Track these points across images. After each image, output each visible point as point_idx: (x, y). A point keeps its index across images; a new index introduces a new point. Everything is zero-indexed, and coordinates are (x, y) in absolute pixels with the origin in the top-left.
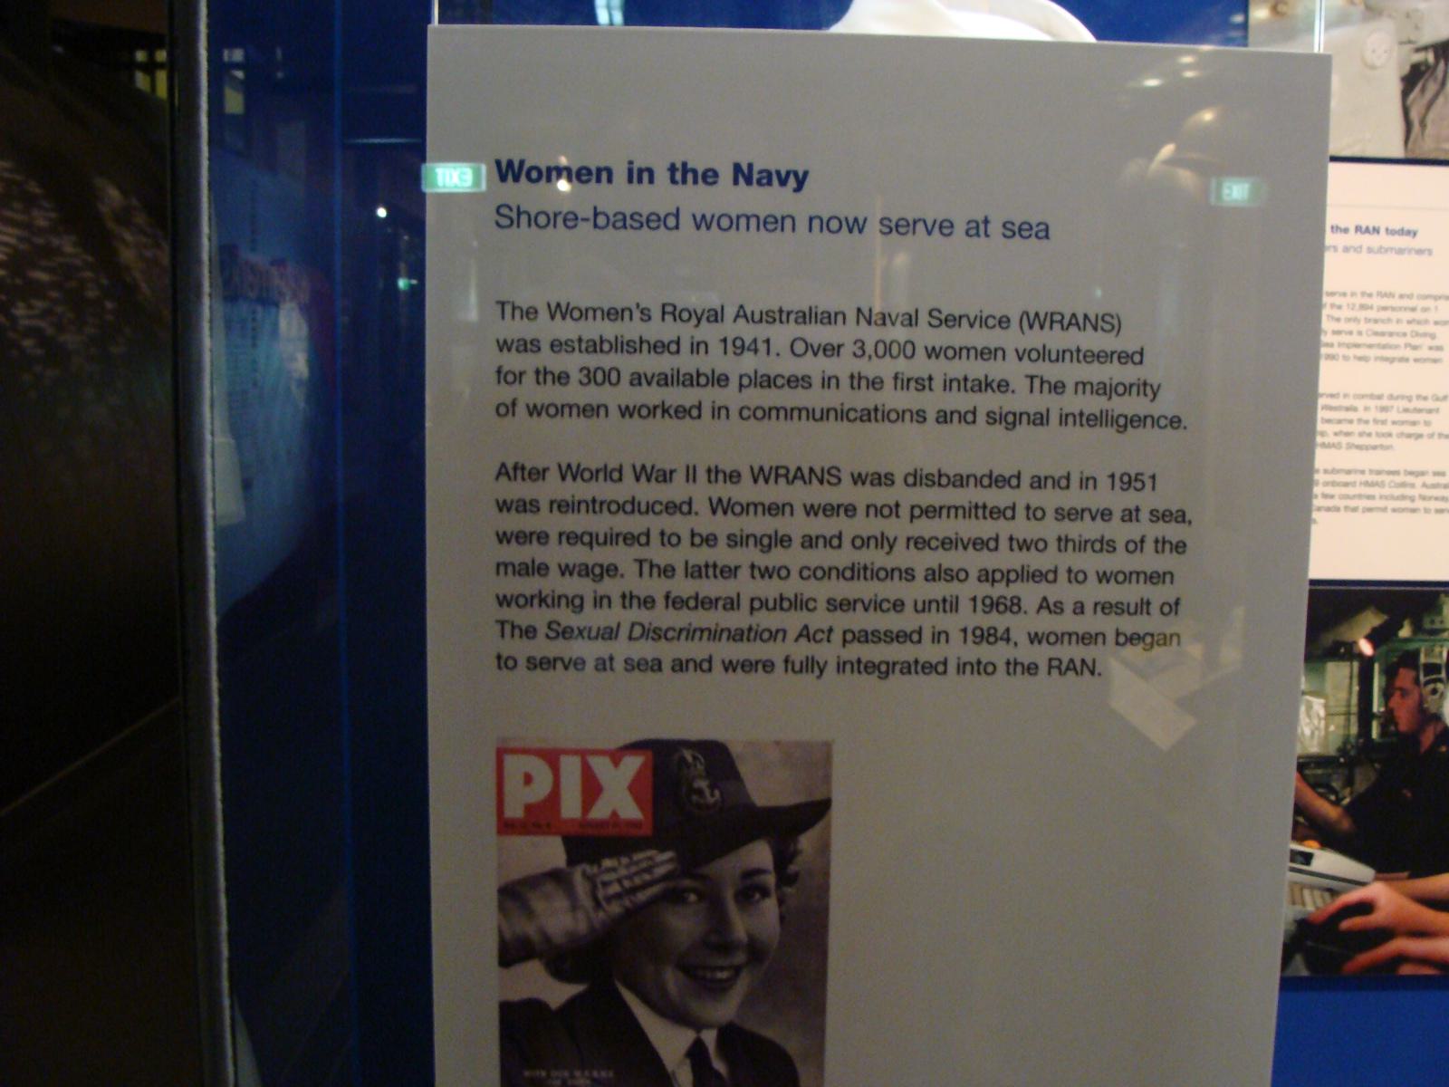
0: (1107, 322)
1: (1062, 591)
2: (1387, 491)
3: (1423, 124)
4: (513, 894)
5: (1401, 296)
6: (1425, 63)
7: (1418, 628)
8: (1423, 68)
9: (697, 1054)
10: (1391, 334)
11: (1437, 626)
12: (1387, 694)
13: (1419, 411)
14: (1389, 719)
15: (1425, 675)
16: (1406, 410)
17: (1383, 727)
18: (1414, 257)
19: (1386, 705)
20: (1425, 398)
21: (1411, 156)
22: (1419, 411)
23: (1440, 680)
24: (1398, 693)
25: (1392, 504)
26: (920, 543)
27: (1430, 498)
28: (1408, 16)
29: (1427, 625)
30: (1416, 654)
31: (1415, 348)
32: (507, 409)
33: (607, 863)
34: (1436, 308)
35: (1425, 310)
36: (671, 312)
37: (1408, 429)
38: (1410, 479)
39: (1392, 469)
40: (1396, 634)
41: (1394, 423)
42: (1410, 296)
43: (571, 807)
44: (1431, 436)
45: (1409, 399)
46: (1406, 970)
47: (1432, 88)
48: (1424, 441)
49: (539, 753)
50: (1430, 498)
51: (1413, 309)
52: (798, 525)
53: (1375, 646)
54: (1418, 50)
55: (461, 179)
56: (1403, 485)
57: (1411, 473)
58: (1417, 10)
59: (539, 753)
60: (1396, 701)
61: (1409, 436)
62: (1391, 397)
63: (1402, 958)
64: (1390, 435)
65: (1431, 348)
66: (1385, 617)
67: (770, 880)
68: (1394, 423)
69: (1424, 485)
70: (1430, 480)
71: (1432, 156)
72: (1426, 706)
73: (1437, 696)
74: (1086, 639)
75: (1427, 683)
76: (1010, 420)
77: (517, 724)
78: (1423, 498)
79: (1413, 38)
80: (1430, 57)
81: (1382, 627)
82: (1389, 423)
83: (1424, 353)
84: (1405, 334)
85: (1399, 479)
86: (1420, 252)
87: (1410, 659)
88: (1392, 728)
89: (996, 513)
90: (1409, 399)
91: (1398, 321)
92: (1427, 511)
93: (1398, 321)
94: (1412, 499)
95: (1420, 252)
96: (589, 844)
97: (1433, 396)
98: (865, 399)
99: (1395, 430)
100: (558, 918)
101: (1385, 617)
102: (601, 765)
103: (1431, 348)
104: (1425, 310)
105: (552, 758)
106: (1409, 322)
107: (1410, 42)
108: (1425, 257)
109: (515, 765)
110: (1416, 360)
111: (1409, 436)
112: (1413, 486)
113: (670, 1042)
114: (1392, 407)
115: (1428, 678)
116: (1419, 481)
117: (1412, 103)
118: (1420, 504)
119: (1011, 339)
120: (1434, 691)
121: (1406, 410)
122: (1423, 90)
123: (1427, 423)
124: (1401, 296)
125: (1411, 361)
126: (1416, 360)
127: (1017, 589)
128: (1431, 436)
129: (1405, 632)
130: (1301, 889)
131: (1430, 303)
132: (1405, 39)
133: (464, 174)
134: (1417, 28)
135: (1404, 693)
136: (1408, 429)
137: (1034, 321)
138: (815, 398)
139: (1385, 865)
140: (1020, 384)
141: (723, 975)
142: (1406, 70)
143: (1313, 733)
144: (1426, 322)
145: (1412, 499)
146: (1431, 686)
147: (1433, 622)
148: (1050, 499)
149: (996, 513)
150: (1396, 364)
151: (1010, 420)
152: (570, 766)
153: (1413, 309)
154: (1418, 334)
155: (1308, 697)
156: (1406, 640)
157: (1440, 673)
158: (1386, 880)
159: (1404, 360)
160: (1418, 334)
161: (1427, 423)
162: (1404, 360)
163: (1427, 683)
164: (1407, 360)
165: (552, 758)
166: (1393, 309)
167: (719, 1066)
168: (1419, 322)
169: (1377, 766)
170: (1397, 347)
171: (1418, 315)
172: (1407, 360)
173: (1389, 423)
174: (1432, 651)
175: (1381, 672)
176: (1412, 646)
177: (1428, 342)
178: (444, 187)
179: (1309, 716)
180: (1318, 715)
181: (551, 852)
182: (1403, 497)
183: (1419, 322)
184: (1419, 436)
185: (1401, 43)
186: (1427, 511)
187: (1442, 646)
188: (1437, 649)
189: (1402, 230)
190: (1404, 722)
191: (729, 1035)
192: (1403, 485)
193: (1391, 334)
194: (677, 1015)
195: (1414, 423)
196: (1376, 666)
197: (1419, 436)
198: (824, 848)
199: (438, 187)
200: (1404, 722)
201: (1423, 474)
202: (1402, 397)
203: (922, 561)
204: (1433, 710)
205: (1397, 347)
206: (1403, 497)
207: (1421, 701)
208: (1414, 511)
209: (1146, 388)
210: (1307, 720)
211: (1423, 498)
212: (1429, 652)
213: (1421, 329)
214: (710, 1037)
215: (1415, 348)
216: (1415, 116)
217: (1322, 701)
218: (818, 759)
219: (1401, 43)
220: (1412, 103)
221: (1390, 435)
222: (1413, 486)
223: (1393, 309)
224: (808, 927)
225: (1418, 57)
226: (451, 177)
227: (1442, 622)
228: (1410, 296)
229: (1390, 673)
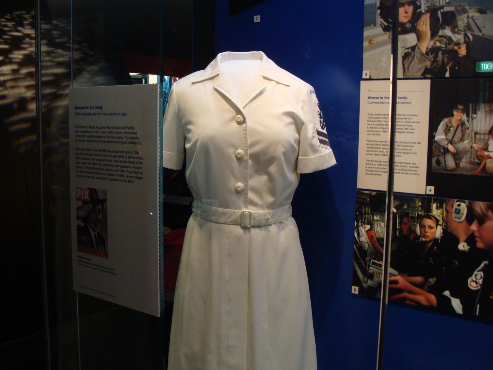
0: (133, 128)
1: (129, 169)
2: (400, 168)
3: (408, 69)
4: (78, 209)
5: (403, 115)
6: (409, 52)
7: (409, 206)
8: (408, 54)
9: (95, 236)
10: (400, 125)
11: (414, 206)
12: (401, 224)
13: (408, 146)
14: (401, 231)
15: (411, 220)
16: (405, 146)
17: (400, 233)
18: (406, 104)
19: (400, 226)
20: (410, 143)
21: (405, 77)
22: (408, 146)
23: (415, 222)
24: (403, 224)
25: (401, 171)
26: (114, 161)
27: (411, 170)
28: (404, 40)
29: (411, 206)
30: (408, 213)
31: (407, 129)
32: (76, 140)
33: (86, 206)
34: (412, 118)
35: (410, 119)
36: (91, 127)
37: (405, 151)
38: (406, 165)
39: (401, 162)
40: (403, 207)
41: (401, 149)
42: (405, 115)
43: (83, 197)
44: (411, 153)
45: (405, 143)
46: (408, 302)
47: (410, 59)
48: (410, 155)
49: (79, 189)
50: (411, 170)
51: (406, 119)
52: (103, 158)
53: (397, 210)
54: (407, 49)
55: (489, 68)
56: (404, 166)
57: (406, 163)
58: (406, 38)
59: (79, 189)
60: (403, 226)
61: (405, 153)
62: (400, 142)
63: (406, 299)
64: (400, 153)
65: (411, 129)
66: (400, 202)
67: (101, 210)
68: (401, 149)
69: (410, 167)
70: (412, 165)
71: (410, 77)
72: (411, 228)
73: (414, 226)
74: (132, 177)
75: (411, 222)
76: (123, 143)
77: (79, 184)
78: (410, 170)
79: (405, 46)
80: (410, 51)
81: (399, 205)
82: (400, 150)
83: (409, 130)
84: (404, 125)
85: (403, 165)
86: (408, 103)
87: (407, 215)
88: (402, 233)
89: (122, 157)
90: (405, 143)
91: (402, 122)
92: (411, 174)
93: (402, 122)
94: (407, 170)
95: (408, 103)
96: (85, 203)
97: (412, 142)
98: (109, 139)
99: (402, 151)
100: (82, 214)
101: (400, 202)
102: (85, 191)
103: (411, 129)
104: (410, 119)
105: (81, 189)
106: (405, 122)
107: (404, 47)
108: (409, 105)
109: (77, 189)
110: (407, 132)
111: (405, 153)
112: (407, 167)
113: (93, 234)
114: (401, 145)
115: (412, 220)
116: (408, 166)
117: (405, 63)
118: (408, 172)
119: (123, 131)
120: (414, 224)
121: (405, 146)
122: (408, 60)
123: (410, 150)
124: (403, 115)
125: (406, 133)
126: (407, 132)
127: (125, 169)
128: (411, 153)
129: (405, 207)
130: (379, 274)
131: (411, 117)
132: (403, 46)
133: (491, 65)
134: (406, 43)
135: (405, 224)
136: (405, 151)
137: (125, 128)
138: (104, 139)
139: (401, 272)
140: (124, 137)
141: (97, 224)
142: (404, 54)
143: (381, 232)
144: (410, 122)
145: (407, 170)
146: (413, 223)
147: (413, 205)
148: (127, 155)
149: (122, 157)
150: (402, 134)
151: (123, 143)
152: (82, 191)
153: (406, 119)
154: (407, 125)
155: (380, 222)
156: (405, 209)
157: (415, 219)
158: (401, 276)
159: (404, 132)
160: (407, 125)
161: (410, 150)
162: (404, 132)
163: (411, 222)
164: (405, 132)
165: (81, 189)
166: (401, 119)
167: (97, 238)
168: (408, 122)
169: (398, 243)
170: (402, 129)
171: (408, 120)
172: (405, 132)
173: (400, 150)
174: (413, 213)
175: (398, 216)
176: (407, 211)
177: (410, 127)
178: (483, 70)
179: (380, 227)
180: (383, 227)
181: (81, 203)
182: (404, 170)
183: (408, 122)
184: (408, 153)
185: (402, 47)
186: (411, 174)
187: (416, 212)
188: (414, 213)
189: (403, 97)
190: (405, 232)
191: (98, 233)
192: (404, 166)
193: (400, 125)
194: (93, 230)
195: (407, 150)
196: (398, 216)
197: (408, 153)
198: (106, 206)
199: (481, 70)
200: (405, 232)
201: (409, 163)
202: (403, 142)
203: (115, 164)
204: (413, 230)
205: (402, 129)
206: (404, 170)
207: (410, 227)
208: (407, 174)
209: (137, 138)
210: (380, 228)
211: (410, 170)
212: (412, 213)
213: (408, 124)
214: (96, 234)
215: (407, 129)
216: (406, 67)
217: (384, 223)
218: (105, 192)
219: (402, 47)
220: (405, 63)
221: (400, 153)
222: (407, 167)
223: (401, 119)
224: (105, 217)
225: (407, 51)
226: (486, 66)
227: (415, 205)
228: (405, 115)
229: (401, 218)
